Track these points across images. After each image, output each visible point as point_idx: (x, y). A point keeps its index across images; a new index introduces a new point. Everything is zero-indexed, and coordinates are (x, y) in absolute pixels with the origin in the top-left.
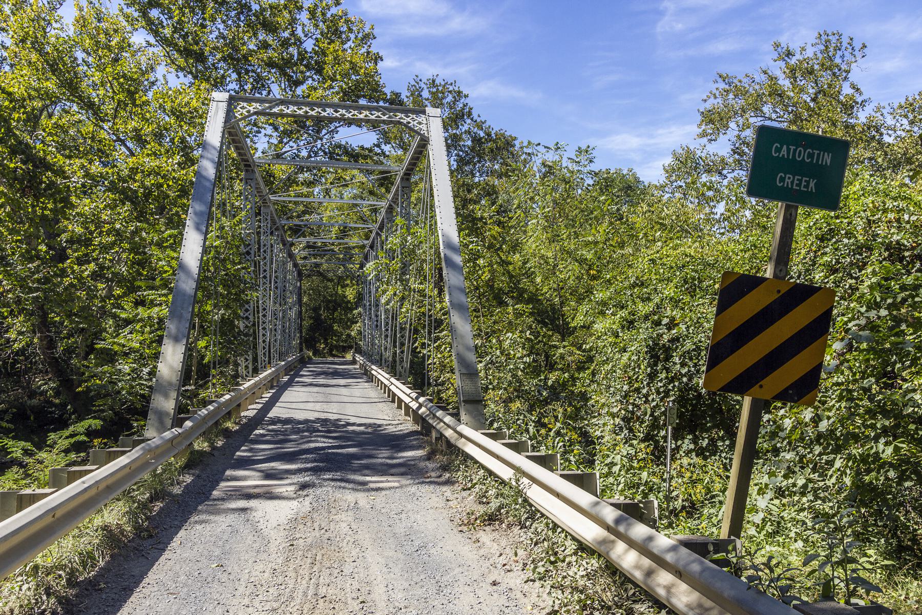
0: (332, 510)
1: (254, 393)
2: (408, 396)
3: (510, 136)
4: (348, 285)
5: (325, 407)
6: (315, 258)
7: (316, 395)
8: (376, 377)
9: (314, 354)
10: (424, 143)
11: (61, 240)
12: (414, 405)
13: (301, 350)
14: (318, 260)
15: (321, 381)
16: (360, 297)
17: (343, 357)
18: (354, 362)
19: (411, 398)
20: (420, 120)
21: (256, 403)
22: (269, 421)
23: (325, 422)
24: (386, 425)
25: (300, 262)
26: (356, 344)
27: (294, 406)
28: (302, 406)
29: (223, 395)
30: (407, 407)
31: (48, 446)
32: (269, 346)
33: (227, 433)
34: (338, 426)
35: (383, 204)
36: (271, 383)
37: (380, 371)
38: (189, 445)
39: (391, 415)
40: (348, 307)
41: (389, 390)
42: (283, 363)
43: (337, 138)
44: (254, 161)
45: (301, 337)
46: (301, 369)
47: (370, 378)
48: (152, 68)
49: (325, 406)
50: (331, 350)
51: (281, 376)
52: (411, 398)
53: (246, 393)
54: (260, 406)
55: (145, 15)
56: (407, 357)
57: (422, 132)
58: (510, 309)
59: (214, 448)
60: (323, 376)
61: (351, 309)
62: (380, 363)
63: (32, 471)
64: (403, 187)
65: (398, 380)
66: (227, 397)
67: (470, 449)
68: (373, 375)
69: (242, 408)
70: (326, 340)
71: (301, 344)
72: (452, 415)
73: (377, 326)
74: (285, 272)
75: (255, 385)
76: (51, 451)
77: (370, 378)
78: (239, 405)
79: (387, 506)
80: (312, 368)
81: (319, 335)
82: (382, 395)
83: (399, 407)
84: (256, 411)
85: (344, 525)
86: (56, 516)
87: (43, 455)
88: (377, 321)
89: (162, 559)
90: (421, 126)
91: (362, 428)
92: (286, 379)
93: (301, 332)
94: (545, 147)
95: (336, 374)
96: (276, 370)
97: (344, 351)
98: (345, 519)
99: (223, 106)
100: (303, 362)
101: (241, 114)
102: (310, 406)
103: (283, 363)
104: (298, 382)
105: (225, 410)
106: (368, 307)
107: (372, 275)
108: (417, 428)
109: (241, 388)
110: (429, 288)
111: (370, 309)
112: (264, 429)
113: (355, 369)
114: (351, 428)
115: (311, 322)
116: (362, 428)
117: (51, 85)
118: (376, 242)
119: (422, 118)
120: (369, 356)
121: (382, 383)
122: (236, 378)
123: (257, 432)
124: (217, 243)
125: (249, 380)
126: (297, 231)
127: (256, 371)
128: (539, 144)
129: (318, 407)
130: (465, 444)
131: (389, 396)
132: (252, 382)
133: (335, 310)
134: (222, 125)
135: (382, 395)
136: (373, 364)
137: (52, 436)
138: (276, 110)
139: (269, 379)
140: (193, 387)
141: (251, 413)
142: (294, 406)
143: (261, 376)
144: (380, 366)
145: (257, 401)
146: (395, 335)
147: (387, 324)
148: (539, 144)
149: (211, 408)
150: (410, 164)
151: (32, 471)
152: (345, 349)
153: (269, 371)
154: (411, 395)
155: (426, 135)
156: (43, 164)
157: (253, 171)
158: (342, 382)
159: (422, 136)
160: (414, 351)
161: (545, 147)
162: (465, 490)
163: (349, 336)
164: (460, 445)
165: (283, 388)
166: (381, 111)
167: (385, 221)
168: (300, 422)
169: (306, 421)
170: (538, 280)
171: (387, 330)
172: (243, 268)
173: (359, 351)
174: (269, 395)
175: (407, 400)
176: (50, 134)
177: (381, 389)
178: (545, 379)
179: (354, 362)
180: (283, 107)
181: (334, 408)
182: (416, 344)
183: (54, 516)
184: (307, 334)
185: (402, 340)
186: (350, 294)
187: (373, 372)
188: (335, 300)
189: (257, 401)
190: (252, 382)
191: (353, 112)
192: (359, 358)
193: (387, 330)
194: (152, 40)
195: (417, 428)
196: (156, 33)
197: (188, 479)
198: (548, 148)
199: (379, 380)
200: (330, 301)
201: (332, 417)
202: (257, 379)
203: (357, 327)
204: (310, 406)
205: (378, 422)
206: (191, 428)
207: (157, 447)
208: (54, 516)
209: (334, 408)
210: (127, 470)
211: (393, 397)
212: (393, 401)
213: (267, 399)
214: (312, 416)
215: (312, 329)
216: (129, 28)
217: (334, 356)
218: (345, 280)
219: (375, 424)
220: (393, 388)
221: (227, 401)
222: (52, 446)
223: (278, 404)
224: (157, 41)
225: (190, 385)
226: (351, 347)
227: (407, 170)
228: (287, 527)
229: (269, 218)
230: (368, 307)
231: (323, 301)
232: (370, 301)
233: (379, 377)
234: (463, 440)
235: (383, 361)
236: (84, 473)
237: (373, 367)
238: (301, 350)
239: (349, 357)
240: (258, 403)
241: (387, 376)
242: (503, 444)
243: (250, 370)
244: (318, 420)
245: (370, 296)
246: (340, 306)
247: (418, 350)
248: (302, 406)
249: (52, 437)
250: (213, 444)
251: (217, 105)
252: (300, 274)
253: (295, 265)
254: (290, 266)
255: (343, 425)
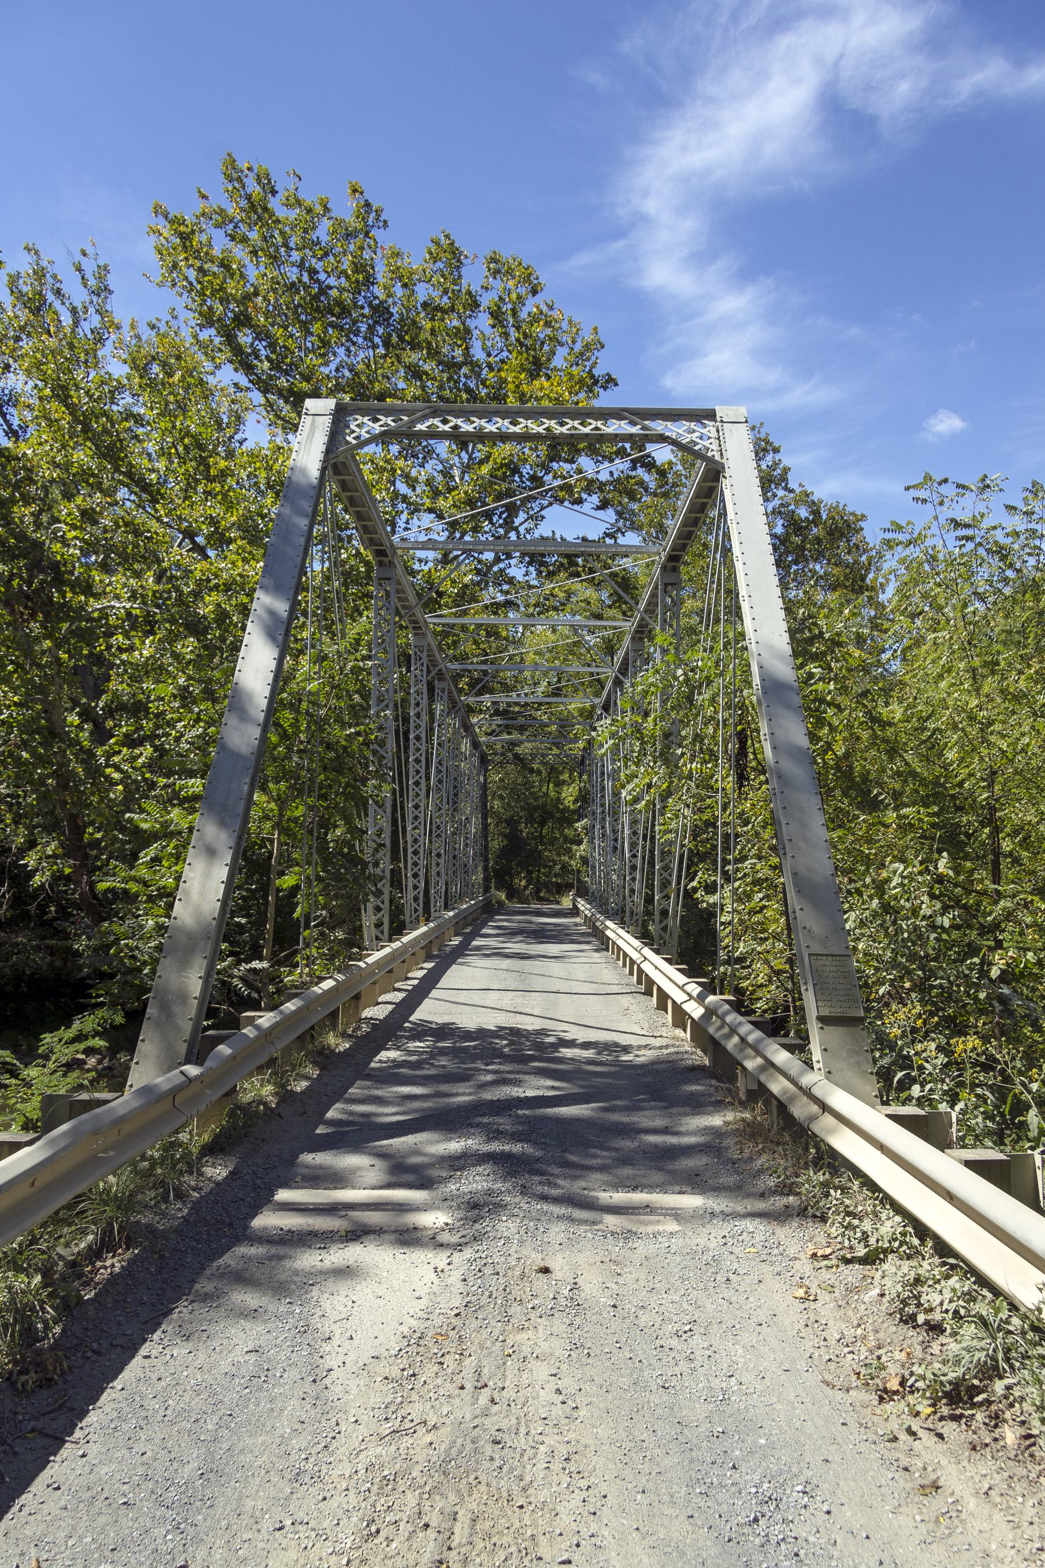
0: (515, 1310)
1: (390, 971)
2: (682, 988)
3: (853, 514)
4: (564, 781)
5: (519, 1001)
6: (509, 733)
7: (505, 974)
8: (614, 943)
9: (509, 897)
10: (715, 473)
11: (97, 706)
12: (696, 1011)
13: (487, 889)
14: (515, 736)
15: (516, 946)
16: (584, 797)
17: (558, 903)
18: (575, 912)
19: (689, 994)
20: (704, 431)
21: (395, 990)
22: (411, 1029)
23: (515, 1034)
24: (639, 1048)
25: (483, 739)
26: (579, 880)
27: (462, 997)
28: (476, 998)
29: (321, 979)
30: (678, 1009)
31: (41, 1056)
32: (427, 883)
33: (325, 1058)
34: (540, 1047)
35: (628, 626)
36: (428, 949)
37: (621, 931)
38: (227, 1095)
39: (646, 1025)
40: (567, 818)
41: (641, 971)
42: (451, 914)
43: (544, 530)
44: (392, 545)
45: (486, 869)
46: (484, 924)
47: (604, 944)
48: (238, 418)
49: (519, 1000)
50: (538, 891)
51: (447, 937)
52: (689, 994)
53: (373, 973)
54: (400, 996)
55: (230, 339)
56: (675, 907)
57: (710, 454)
58: (891, 816)
59: (285, 1096)
60: (519, 938)
61: (570, 823)
62: (621, 917)
63: (14, 1100)
64: (666, 585)
65: (657, 952)
66: (328, 984)
67: (845, 1143)
68: (608, 939)
69: (362, 1002)
70: (530, 872)
71: (487, 879)
72: (790, 1048)
73: (615, 849)
74: (456, 754)
75: (393, 955)
76: (44, 1066)
77: (604, 944)
78: (357, 997)
79: (653, 1301)
80: (501, 920)
81: (517, 865)
82: (626, 980)
83: (662, 1006)
84: (390, 1007)
85: (541, 1372)
86: (36, 1184)
87: (32, 1072)
88: (616, 840)
89: (38, 1486)
90: (707, 443)
91: (589, 1054)
92: (456, 941)
93: (486, 860)
94: (958, 486)
95: (542, 935)
96: (438, 927)
97: (559, 892)
98: (544, 1347)
99: (325, 424)
100: (489, 910)
101: (357, 438)
102: (491, 999)
103: (451, 914)
104: (478, 948)
105: (324, 1012)
106: (599, 817)
107: (606, 746)
108: (701, 1058)
109: (362, 964)
110: (724, 779)
111: (604, 819)
112: (398, 1048)
113: (576, 925)
114: (567, 1052)
115: (506, 842)
116: (589, 1054)
117: (82, 456)
118: (613, 699)
119: (710, 429)
120: (600, 902)
121: (625, 955)
122: (354, 943)
123: (384, 1055)
124: (313, 686)
125: (383, 947)
126: (480, 686)
127: (398, 929)
128: (946, 481)
129: (506, 1000)
130: (832, 1131)
131: (639, 982)
132: (387, 951)
133: (542, 824)
134: (321, 456)
135: (626, 980)
136: (608, 918)
137: (47, 1038)
138: (421, 427)
139: (423, 943)
140: (265, 964)
141: (378, 1012)
142: (462, 997)
143: (405, 939)
144: (622, 923)
145: (397, 985)
146: (652, 864)
147: (633, 845)
148: (946, 481)
149: (290, 1006)
150: (679, 537)
151: (14, 1100)
152: (562, 889)
153: (423, 929)
154: (688, 988)
155: (717, 458)
156: (57, 572)
157: (391, 564)
158: (553, 949)
159: (711, 460)
160: (689, 895)
161: (958, 486)
162: (847, 1262)
163: (565, 867)
164: (816, 1128)
165: (446, 960)
166: (625, 418)
167: (631, 655)
168: (468, 1035)
169: (481, 1034)
170: (951, 755)
171: (634, 856)
172: (358, 734)
173: (583, 892)
174: (420, 974)
175: (679, 996)
176: (74, 527)
177: (624, 965)
178: (982, 964)
179: (575, 912)
180: (436, 421)
181: (536, 1004)
182: (695, 884)
183: (33, 1184)
184: (496, 863)
185: (665, 875)
186: (569, 795)
187: (608, 933)
188: (544, 805)
189: (397, 985)
190: (387, 951)
191: (571, 423)
192: (582, 905)
193: (634, 856)
194: (243, 380)
195: (701, 1058)
196: (248, 368)
197: (217, 1171)
198: (964, 487)
199: (619, 949)
200: (535, 809)
201: (530, 1024)
202: (396, 945)
203: (582, 850)
204: (491, 999)
205: (624, 1040)
206: (233, 1057)
207: (121, 1121)
208: (33, 1184)
209: (536, 1004)
210: (25, 1190)
211: (648, 986)
212: (648, 993)
213: (416, 982)
214: (490, 1021)
215: (505, 853)
216: (208, 366)
217: (541, 900)
218: (562, 773)
219: (616, 1044)
220: (646, 967)
221: (326, 993)
222: (46, 1057)
223: (434, 993)
224: (251, 381)
225: (261, 960)
226: (569, 887)
227: (673, 549)
228: (395, 1372)
229: (424, 656)
230: (599, 817)
231: (523, 808)
232: (603, 805)
233: (620, 943)
234: (828, 1120)
235: (628, 913)
236: (5, 1149)
237: (609, 923)
238: (487, 889)
239: (566, 902)
240: (399, 990)
241: (636, 943)
242: (970, 1164)
243: (386, 927)
244: (501, 1032)
245: (603, 797)
246: (552, 816)
247: (698, 895)
248: (476, 998)
249: (48, 1040)
250: (283, 1087)
251: (313, 422)
252: (484, 760)
253: (476, 744)
254: (465, 746)
255: (552, 1045)
